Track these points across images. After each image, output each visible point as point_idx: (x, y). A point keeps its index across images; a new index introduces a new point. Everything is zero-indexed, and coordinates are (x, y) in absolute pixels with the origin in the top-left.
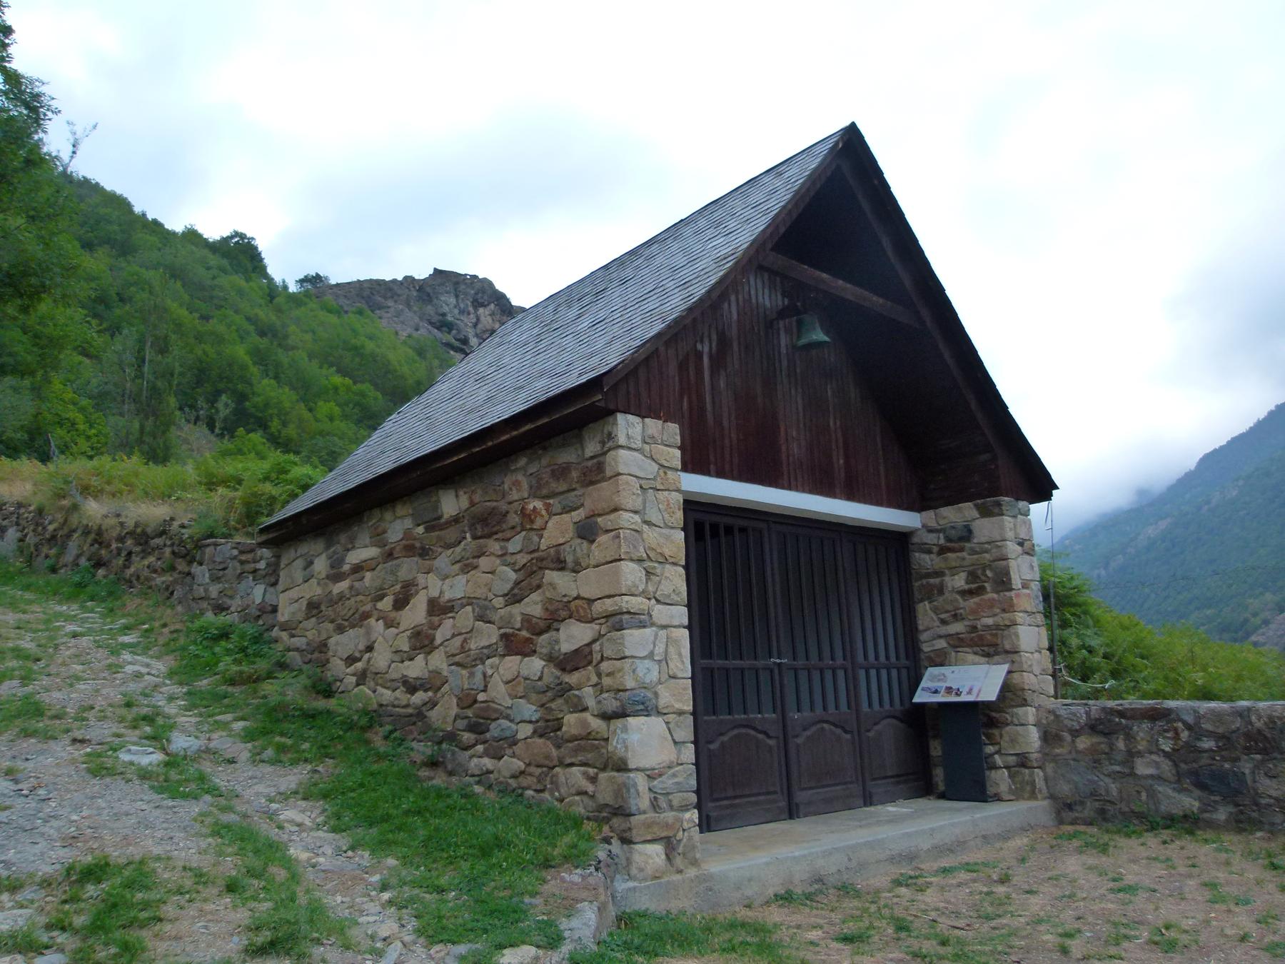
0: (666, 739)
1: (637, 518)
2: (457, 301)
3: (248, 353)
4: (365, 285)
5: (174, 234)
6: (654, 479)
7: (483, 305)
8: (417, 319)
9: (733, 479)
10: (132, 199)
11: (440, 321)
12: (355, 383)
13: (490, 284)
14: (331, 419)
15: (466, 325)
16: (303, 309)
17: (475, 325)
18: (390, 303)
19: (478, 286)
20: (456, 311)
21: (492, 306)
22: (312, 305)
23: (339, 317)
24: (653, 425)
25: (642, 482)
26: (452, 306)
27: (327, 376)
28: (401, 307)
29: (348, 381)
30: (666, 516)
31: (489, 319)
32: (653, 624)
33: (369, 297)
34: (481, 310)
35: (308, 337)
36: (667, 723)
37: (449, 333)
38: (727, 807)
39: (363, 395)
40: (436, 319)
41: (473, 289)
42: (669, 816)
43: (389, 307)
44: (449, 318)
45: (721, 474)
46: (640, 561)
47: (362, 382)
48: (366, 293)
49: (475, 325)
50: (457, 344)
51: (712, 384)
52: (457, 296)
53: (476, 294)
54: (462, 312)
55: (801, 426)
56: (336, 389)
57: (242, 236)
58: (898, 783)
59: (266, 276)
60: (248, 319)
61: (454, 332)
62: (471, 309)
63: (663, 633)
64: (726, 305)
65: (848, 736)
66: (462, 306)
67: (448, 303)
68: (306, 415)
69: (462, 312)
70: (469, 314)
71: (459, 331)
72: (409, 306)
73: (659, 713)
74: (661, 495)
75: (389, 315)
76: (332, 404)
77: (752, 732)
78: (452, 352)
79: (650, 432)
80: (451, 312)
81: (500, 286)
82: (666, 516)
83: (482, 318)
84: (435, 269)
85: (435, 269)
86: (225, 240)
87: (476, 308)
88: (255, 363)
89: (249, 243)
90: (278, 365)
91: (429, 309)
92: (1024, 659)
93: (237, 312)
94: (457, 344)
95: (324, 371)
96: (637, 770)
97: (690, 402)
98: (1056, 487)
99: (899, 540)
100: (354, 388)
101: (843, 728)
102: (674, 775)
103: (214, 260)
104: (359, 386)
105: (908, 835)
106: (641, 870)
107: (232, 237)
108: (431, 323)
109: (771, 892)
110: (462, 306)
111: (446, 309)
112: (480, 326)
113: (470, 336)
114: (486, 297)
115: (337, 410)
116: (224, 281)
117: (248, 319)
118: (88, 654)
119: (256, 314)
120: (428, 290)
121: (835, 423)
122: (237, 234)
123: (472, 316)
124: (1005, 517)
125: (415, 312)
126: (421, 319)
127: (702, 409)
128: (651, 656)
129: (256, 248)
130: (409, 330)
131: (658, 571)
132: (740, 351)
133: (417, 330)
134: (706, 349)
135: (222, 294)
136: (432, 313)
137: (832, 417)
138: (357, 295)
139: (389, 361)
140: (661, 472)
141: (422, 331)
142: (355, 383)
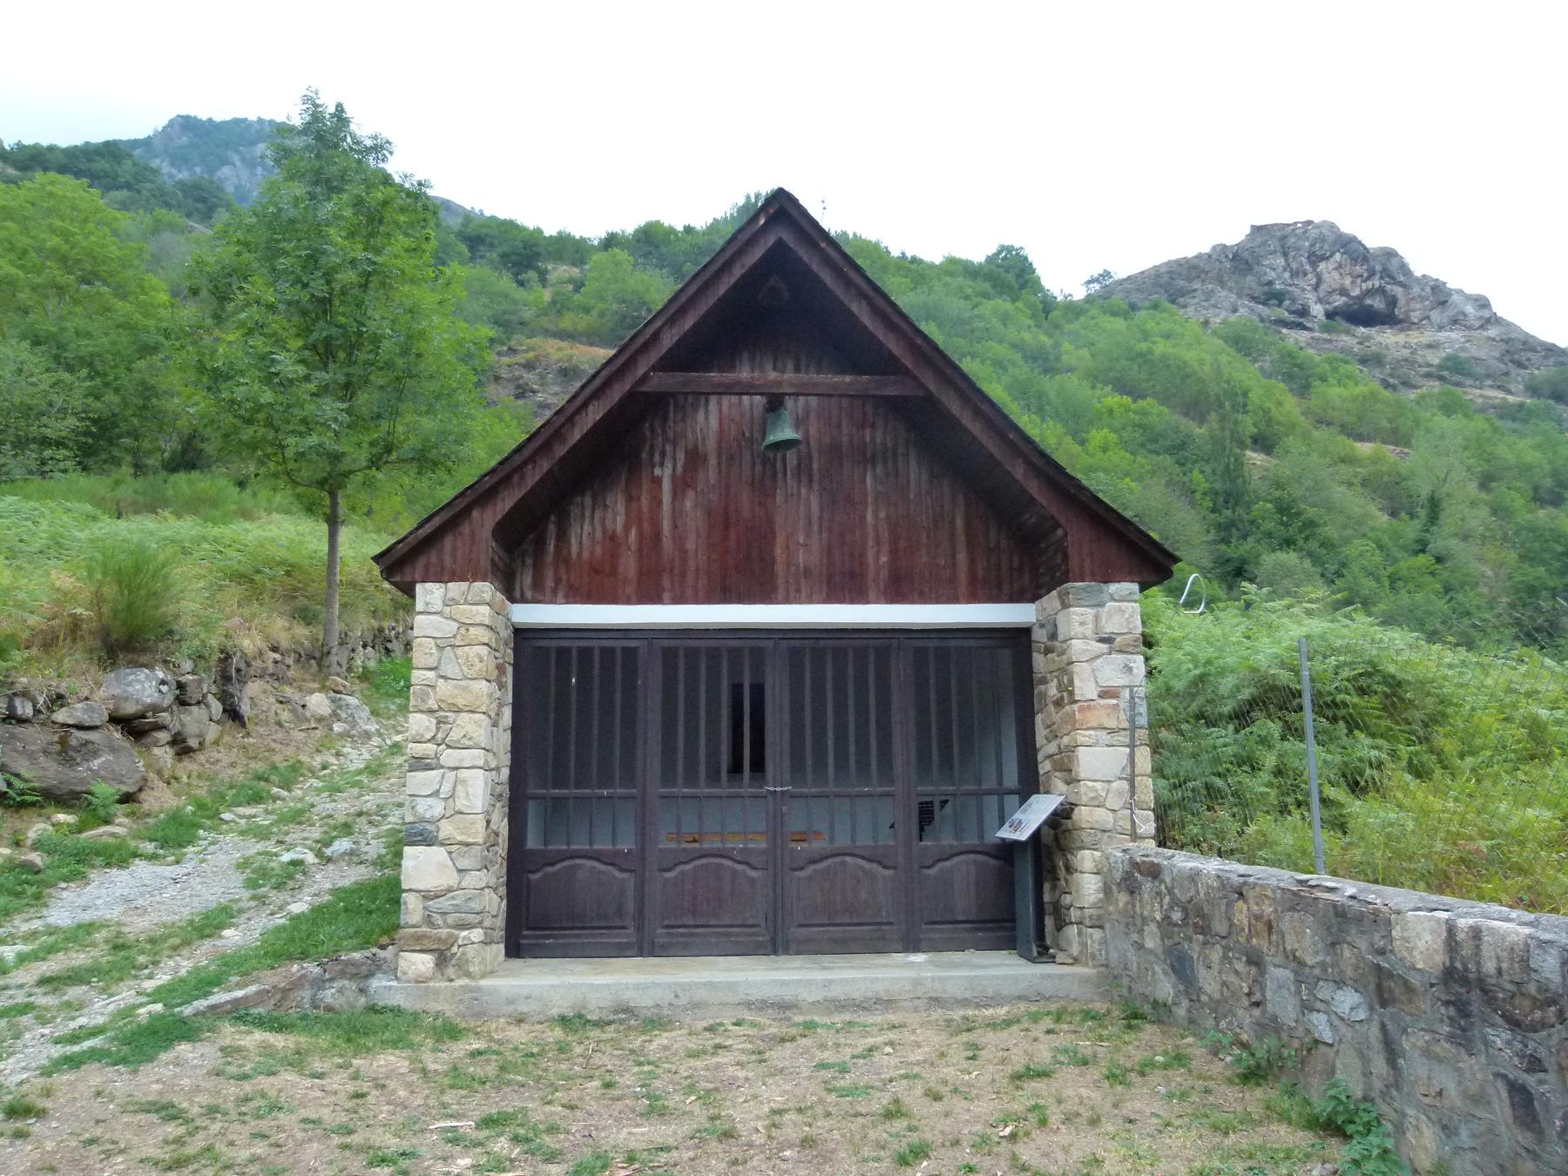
0: (446, 866)
1: (431, 674)
2: (1286, 260)
3: (1008, 388)
4: (1162, 270)
5: (932, 266)
6: (454, 637)
7: (1324, 258)
8: (1233, 297)
9: (703, 602)
10: (885, 242)
11: (1265, 293)
12: (1135, 401)
13: (1332, 226)
14: (1105, 449)
15: (1304, 290)
16: (1082, 319)
17: (1316, 288)
18: (1197, 285)
19: (1313, 233)
20: (1287, 275)
21: (1338, 256)
22: (1094, 312)
23: (1126, 319)
24: (456, 588)
25: (439, 641)
26: (1280, 270)
27: (1099, 398)
28: (1210, 286)
29: (1127, 400)
30: (465, 669)
31: (1336, 275)
32: (442, 767)
33: (1169, 284)
34: (1322, 266)
35: (1085, 352)
36: (450, 853)
37: (1280, 305)
38: (682, 935)
39: (1144, 413)
40: (1259, 291)
41: (1307, 239)
42: (444, 932)
43: (1195, 290)
44: (1278, 286)
45: (679, 599)
46: (431, 711)
47: (1144, 397)
48: (1166, 278)
49: (1316, 288)
50: (1292, 318)
51: (674, 510)
52: (1285, 255)
53: (1313, 245)
54: (1295, 274)
55: (815, 528)
56: (1111, 412)
57: (1009, 249)
58: (977, 930)
59: (1040, 288)
60: (1014, 346)
61: (1287, 303)
62: (1308, 267)
63: (451, 775)
64: (701, 415)
65: (889, 872)
66: (1294, 266)
67: (1274, 268)
68: (1076, 448)
69: (1295, 274)
70: (1305, 274)
71: (1293, 301)
72: (1222, 283)
73: (442, 844)
74: (459, 651)
75: (1196, 300)
76: (1106, 430)
77: (729, 863)
78: (1285, 331)
79: (450, 595)
80: (1279, 278)
81: (1346, 228)
82: (465, 669)
83: (1325, 276)
84: (1253, 227)
85: (1253, 227)
86: (991, 260)
87: (1314, 265)
88: (1015, 399)
89: (1017, 254)
90: (1041, 395)
91: (1250, 281)
92: (1083, 790)
93: (1000, 342)
94: (1292, 318)
95: (1098, 392)
96: (410, 890)
97: (640, 535)
98: (1176, 560)
99: (1019, 637)
100: (1133, 406)
101: (880, 863)
102: (453, 898)
103: (970, 287)
104: (1141, 403)
105: (783, 983)
106: (405, 973)
107: (999, 253)
108: (1254, 299)
109: (555, 1012)
110: (1294, 266)
111: (1272, 275)
112: (1323, 287)
113: (1311, 303)
114: (1326, 247)
115: (1113, 437)
116: (987, 307)
117: (1014, 346)
118: (420, 764)
119: (1022, 339)
120: (1246, 255)
121: (876, 517)
122: (1003, 248)
123: (1310, 276)
124: (1072, 609)
125: (1230, 290)
126: (1239, 296)
127: (657, 535)
128: (436, 794)
129: (1026, 259)
130: (1223, 314)
131: (451, 720)
132: (719, 464)
133: (1235, 311)
134: (668, 472)
135: (982, 324)
136: (1254, 285)
137: (870, 509)
138: (1154, 284)
139: (1184, 362)
140: (463, 631)
141: (1242, 311)
142: (1135, 401)
